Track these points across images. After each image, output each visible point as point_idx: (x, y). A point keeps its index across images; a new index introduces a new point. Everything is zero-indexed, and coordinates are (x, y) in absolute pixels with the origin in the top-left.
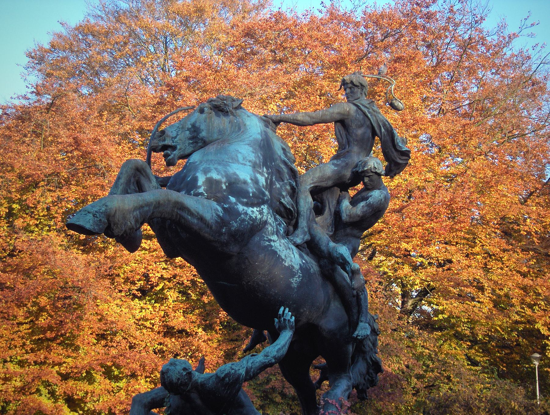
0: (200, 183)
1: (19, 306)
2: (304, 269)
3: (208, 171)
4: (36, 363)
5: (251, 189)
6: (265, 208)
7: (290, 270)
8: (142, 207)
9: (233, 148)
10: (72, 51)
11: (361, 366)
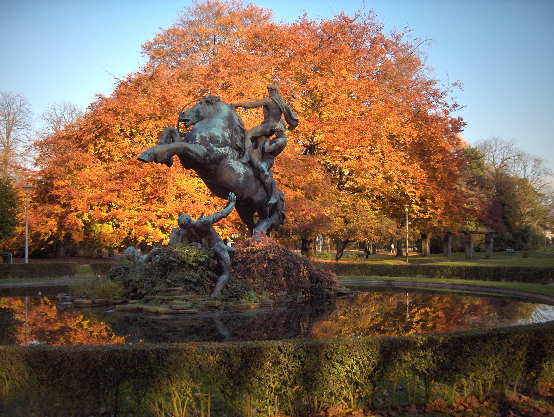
0: (197, 138)
1: (136, 182)
2: (246, 174)
3: (201, 131)
4: (145, 210)
5: (221, 140)
6: (227, 148)
7: (239, 175)
8: (169, 150)
9: (214, 120)
10: (166, 44)
11: (276, 216)
